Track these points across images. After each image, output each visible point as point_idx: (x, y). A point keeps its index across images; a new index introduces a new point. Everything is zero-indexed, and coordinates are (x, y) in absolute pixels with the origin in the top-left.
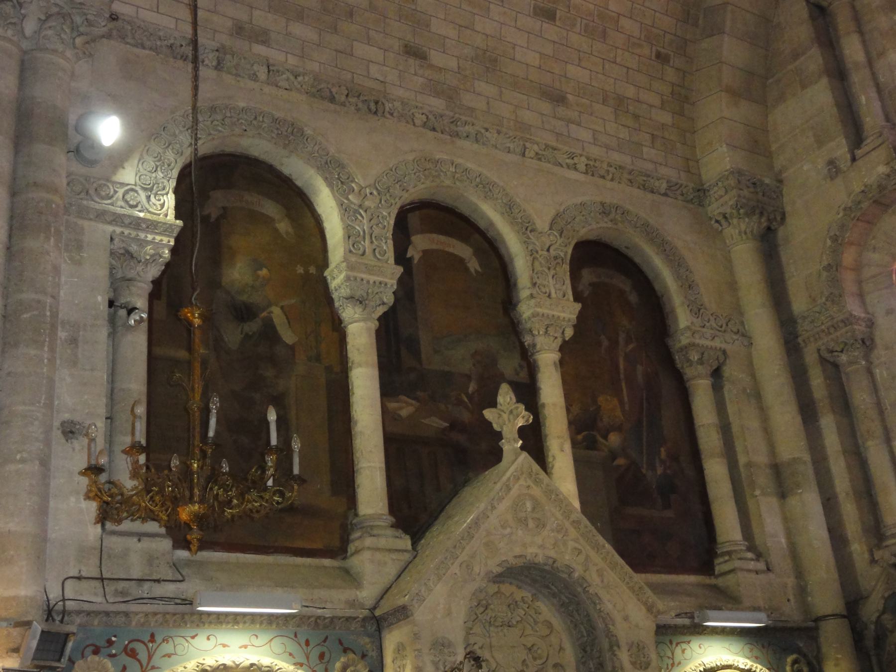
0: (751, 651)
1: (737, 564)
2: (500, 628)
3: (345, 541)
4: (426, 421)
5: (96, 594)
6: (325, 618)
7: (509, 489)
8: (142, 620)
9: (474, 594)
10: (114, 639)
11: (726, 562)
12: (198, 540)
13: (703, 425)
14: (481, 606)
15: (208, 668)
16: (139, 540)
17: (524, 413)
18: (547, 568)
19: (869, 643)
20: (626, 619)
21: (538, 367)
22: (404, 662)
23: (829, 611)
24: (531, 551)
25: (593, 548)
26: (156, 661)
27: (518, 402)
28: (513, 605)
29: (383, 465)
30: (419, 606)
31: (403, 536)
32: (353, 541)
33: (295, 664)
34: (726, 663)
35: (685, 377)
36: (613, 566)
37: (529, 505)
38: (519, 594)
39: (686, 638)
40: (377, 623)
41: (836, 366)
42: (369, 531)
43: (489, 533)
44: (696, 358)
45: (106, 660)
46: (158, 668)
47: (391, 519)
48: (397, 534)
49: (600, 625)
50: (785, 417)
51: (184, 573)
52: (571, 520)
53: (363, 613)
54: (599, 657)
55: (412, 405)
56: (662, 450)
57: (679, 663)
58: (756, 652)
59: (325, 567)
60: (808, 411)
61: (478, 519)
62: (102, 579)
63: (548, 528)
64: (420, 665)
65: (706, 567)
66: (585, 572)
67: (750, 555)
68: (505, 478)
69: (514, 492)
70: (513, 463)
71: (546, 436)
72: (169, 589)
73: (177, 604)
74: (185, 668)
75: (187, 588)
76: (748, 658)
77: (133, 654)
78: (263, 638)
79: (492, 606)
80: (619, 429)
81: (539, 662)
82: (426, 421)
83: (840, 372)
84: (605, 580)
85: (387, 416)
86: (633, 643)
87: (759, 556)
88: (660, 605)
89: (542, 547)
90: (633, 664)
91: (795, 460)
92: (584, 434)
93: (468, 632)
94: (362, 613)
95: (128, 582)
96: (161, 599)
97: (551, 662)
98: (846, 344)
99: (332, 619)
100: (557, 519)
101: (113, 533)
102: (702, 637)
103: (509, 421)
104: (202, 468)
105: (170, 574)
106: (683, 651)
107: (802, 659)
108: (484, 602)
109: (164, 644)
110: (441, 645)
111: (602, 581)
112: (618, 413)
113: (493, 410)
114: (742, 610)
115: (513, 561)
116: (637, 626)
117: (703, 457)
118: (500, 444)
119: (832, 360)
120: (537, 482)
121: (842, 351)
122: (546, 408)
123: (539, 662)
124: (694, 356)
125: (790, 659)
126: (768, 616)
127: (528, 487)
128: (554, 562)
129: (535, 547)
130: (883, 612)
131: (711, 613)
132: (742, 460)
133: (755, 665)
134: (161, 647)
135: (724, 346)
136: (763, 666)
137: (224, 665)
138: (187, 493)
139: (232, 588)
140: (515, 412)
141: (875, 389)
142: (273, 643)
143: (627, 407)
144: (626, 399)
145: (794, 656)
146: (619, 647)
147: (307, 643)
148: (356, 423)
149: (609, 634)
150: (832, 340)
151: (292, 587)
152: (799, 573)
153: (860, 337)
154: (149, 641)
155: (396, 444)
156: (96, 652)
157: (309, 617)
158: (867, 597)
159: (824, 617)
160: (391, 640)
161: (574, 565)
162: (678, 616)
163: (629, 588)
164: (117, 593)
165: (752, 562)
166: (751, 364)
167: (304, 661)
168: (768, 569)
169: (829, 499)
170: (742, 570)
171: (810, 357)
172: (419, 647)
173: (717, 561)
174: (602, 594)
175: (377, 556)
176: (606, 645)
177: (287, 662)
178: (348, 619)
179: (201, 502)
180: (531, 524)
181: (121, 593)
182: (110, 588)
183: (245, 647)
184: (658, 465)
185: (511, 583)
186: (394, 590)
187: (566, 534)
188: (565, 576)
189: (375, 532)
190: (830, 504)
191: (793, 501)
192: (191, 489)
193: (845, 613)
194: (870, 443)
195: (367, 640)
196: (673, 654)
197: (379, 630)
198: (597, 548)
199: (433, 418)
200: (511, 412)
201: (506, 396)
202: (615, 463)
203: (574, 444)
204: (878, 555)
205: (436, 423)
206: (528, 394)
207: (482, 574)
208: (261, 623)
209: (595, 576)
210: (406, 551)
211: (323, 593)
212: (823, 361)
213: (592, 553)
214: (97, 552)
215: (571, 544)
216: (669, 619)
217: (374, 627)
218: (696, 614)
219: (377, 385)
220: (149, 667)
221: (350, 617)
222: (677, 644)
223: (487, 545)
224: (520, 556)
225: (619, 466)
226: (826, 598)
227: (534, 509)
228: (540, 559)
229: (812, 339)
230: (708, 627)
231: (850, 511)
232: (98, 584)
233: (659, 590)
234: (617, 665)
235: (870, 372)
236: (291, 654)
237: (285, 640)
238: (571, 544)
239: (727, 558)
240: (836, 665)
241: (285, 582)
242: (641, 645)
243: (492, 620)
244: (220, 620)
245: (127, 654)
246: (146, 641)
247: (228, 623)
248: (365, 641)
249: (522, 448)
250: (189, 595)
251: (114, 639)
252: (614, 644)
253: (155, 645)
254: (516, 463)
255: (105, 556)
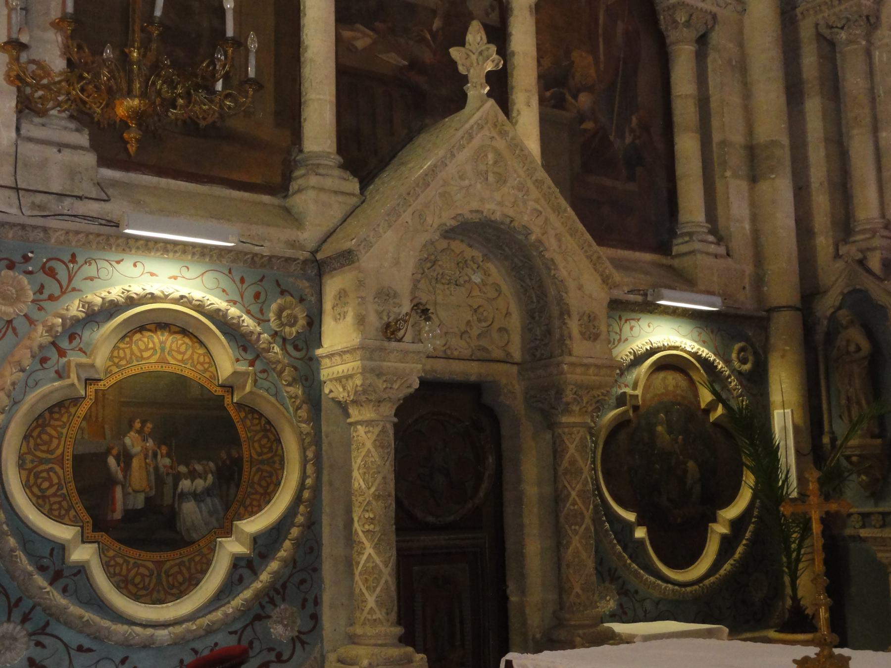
0: (700, 334)
1: (697, 246)
2: (447, 286)
3: (287, 178)
4: (384, 57)
5: (11, 205)
6: (263, 256)
7: (471, 137)
8: (62, 238)
9: (425, 246)
10: (30, 255)
11: (686, 242)
12: (138, 141)
13: (680, 96)
14: (428, 262)
15: (135, 296)
16: (59, 151)
17: (495, 56)
18: (502, 227)
19: (819, 337)
20: (580, 288)
21: (512, 10)
22: (345, 310)
23: (783, 302)
24: (489, 206)
25: (554, 211)
26: (75, 283)
27: (489, 42)
28: (462, 264)
29: (334, 99)
30: (366, 252)
31: (351, 178)
32: (297, 178)
33: (227, 301)
34: (673, 344)
35: (668, 41)
36: (573, 232)
37: (491, 157)
38: (469, 253)
39: (634, 315)
40: (317, 267)
41: (832, 44)
42: (315, 169)
43: (445, 183)
44: (683, 19)
45: (21, 276)
46: (79, 290)
47: (339, 159)
48: (345, 176)
49: (552, 292)
50: (769, 95)
51: (109, 193)
52: (534, 178)
53: (302, 255)
54: (547, 325)
55: (368, 36)
56: (634, 119)
57: (626, 340)
58: (704, 336)
59: (265, 204)
60: (794, 92)
61: (435, 166)
62: (17, 189)
63: (508, 184)
64: (364, 313)
65: (663, 248)
66: (543, 234)
67: (711, 238)
68: (467, 126)
69: (477, 141)
70: (478, 110)
71: (512, 88)
72: (93, 208)
73: (101, 224)
74: (109, 293)
75: (114, 209)
76: (696, 342)
77: (52, 273)
78: (195, 271)
79: (440, 263)
80: (590, 89)
81: (484, 324)
82: (384, 57)
83: (835, 52)
84: (564, 247)
85: (341, 45)
86: (584, 313)
87: (720, 240)
88: (617, 277)
89: (500, 204)
90: (582, 334)
91: (773, 143)
92: (552, 91)
93: (415, 287)
94: (302, 255)
95: (47, 195)
96: (84, 217)
97: (496, 326)
98: (848, 20)
99: (271, 258)
100: (519, 176)
101: (30, 139)
102: (652, 316)
103: (478, 64)
104: (144, 56)
105: (94, 192)
106: (632, 328)
107: (749, 348)
108: (433, 257)
109: (86, 266)
110: (385, 295)
111: (560, 247)
112: (592, 71)
113: (462, 49)
114: (697, 292)
115: (468, 216)
116: (590, 296)
117: (676, 130)
118: (465, 88)
119: (829, 37)
120: (503, 134)
121: (842, 28)
122: (516, 57)
123: (484, 324)
124: (682, 18)
125: (737, 346)
126: (723, 303)
127: (492, 138)
128: (511, 221)
129: (492, 203)
130: (839, 308)
131: (665, 292)
132: (716, 137)
133: (702, 349)
134: (83, 268)
135: (715, 9)
136: (710, 351)
137: (152, 294)
138: (124, 86)
139: (166, 215)
140: (485, 54)
141: (871, 73)
142: (205, 276)
143: (602, 66)
144: (602, 57)
145: (741, 344)
146: (569, 316)
147: (242, 280)
148: (306, 50)
149: (560, 300)
150: (834, 14)
151: (228, 220)
152: (759, 259)
153: (865, 12)
154: (70, 261)
155: (350, 79)
156: (11, 266)
157: (246, 254)
158: (825, 292)
159: (778, 309)
160: (332, 286)
161: (533, 227)
162: (630, 292)
163: (587, 257)
164: (34, 206)
165: (713, 246)
166: (741, 32)
167: (237, 298)
168: (728, 255)
169: (800, 188)
170: (702, 252)
171: (806, 31)
172: (363, 294)
173: (675, 242)
174: (558, 259)
175: (320, 198)
176: (555, 311)
177: (219, 298)
178: (288, 260)
179: (143, 95)
180: (491, 178)
181: (39, 206)
182: (27, 199)
183: (175, 278)
184: (627, 134)
185: (462, 241)
186: (340, 234)
187: (527, 193)
188: (520, 237)
189: (322, 171)
190: (801, 192)
191: (764, 186)
192: (130, 82)
193: (799, 306)
194: (855, 132)
195: (307, 284)
196: (621, 330)
197: (320, 275)
198: (557, 210)
199: (393, 55)
200: (481, 53)
201: (475, 35)
202: (584, 126)
203: (542, 101)
204: (843, 250)
205: (394, 59)
206: (499, 35)
207: (435, 226)
208: (194, 254)
209: (553, 241)
210: (354, 195)
211: (261, 230)
212: (820, 36)
213: (553, 217)
214: (12, 159)
215: (531, 204)
216: (618, 294)
217: (315, 271)
218: (650, 291)
219: (333, 9)
220: (70, 289)
221: (290, 258)
222: (626, 321)
223: (443, 195)
224: (477, 211)
225: (585, 130)
226: (783, 289)
227: (495, 163)
228: (497, 216)
229: (812, 12)
230: (660, 305)
231: (821, 203)
232: (12, 194)
233: (619, 265)
234: (566, 333)
235: (869, 54)
236: (224, 291)
237: (216, 275)
238: (531, 204)
239: (687, 239)
240: (783, 357)
241: (219, 215)
242: (592, 316)
243: (439, 277)
244: (149, 246)
245: (45, 272)
246: (66, 261)
247: (157, 250)
248: (304, 285)
249: (489, 95)
250: (114, 217)
251: (30, 255)
252: (565, 312)
253: (76, 267)
254: (481, 110)
255: (20, 164)
